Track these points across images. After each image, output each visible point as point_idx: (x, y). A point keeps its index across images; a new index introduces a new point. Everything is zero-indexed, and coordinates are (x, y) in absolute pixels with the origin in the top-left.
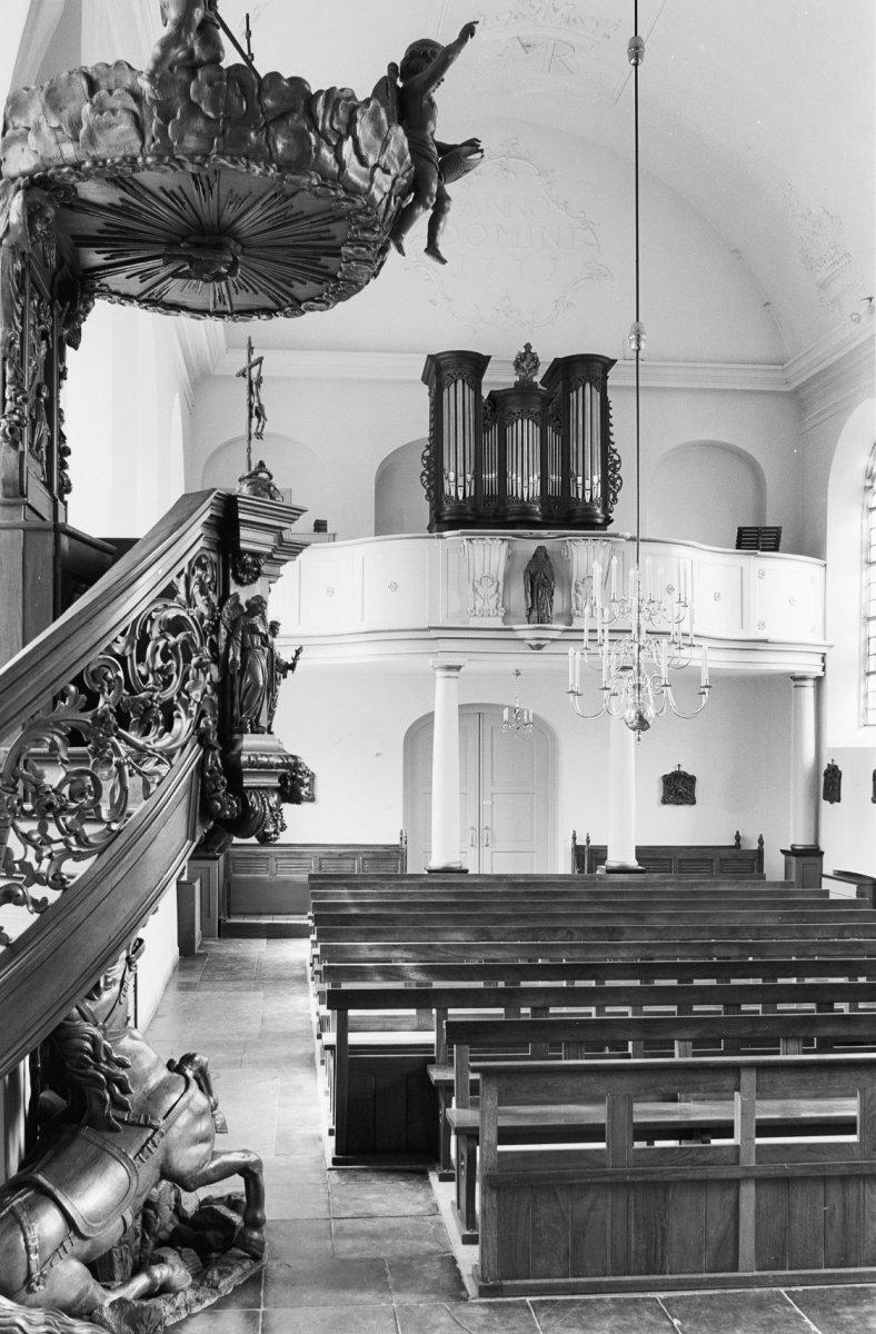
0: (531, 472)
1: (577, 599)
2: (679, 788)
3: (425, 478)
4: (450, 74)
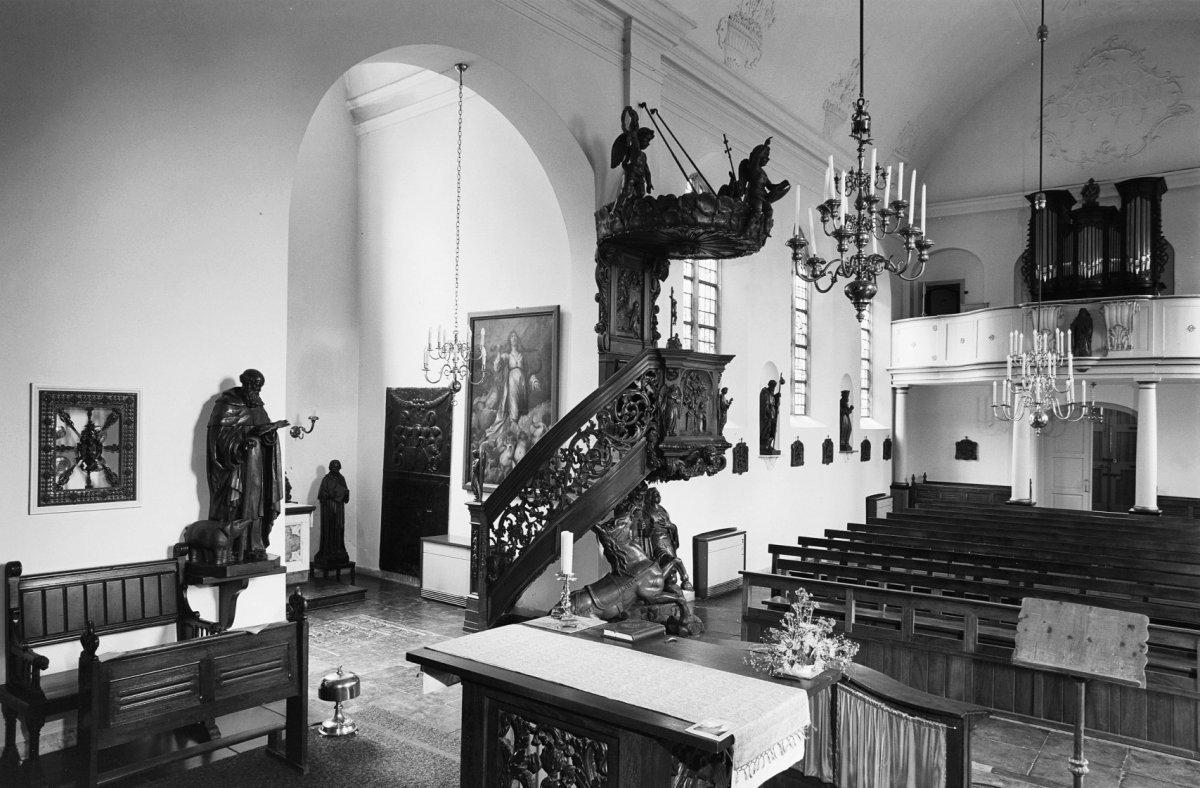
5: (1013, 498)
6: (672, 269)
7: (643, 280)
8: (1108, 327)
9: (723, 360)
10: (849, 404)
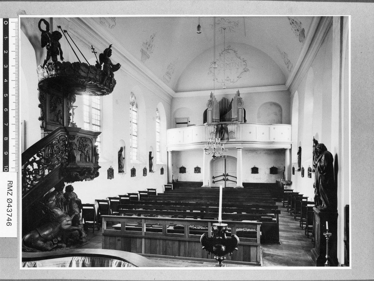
2: (255, 170)
4: (36, 64)
5: (203, 186)
6: (77, 98)
7: (63, 101)
9: (97, 134)
10: (152, 156)
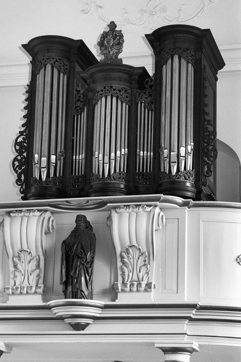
0: (118, 146)
1: (123, 273)
3: (16, 163)
8: (118, 250)
